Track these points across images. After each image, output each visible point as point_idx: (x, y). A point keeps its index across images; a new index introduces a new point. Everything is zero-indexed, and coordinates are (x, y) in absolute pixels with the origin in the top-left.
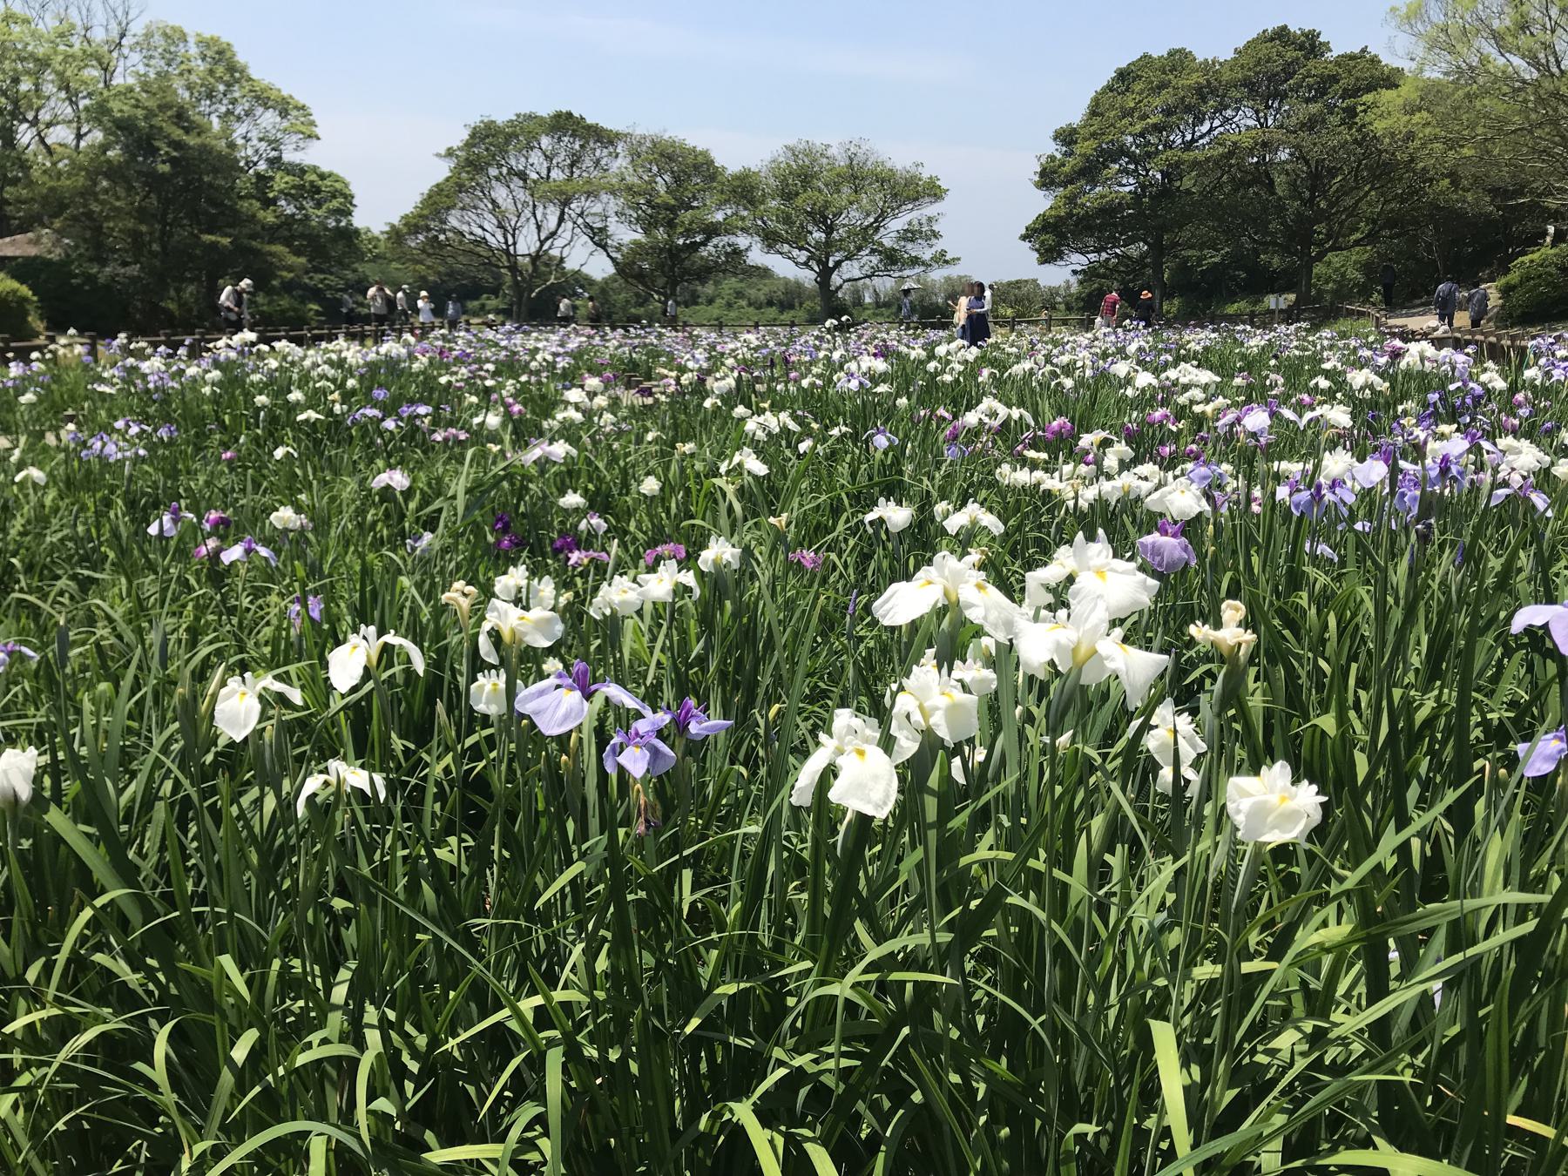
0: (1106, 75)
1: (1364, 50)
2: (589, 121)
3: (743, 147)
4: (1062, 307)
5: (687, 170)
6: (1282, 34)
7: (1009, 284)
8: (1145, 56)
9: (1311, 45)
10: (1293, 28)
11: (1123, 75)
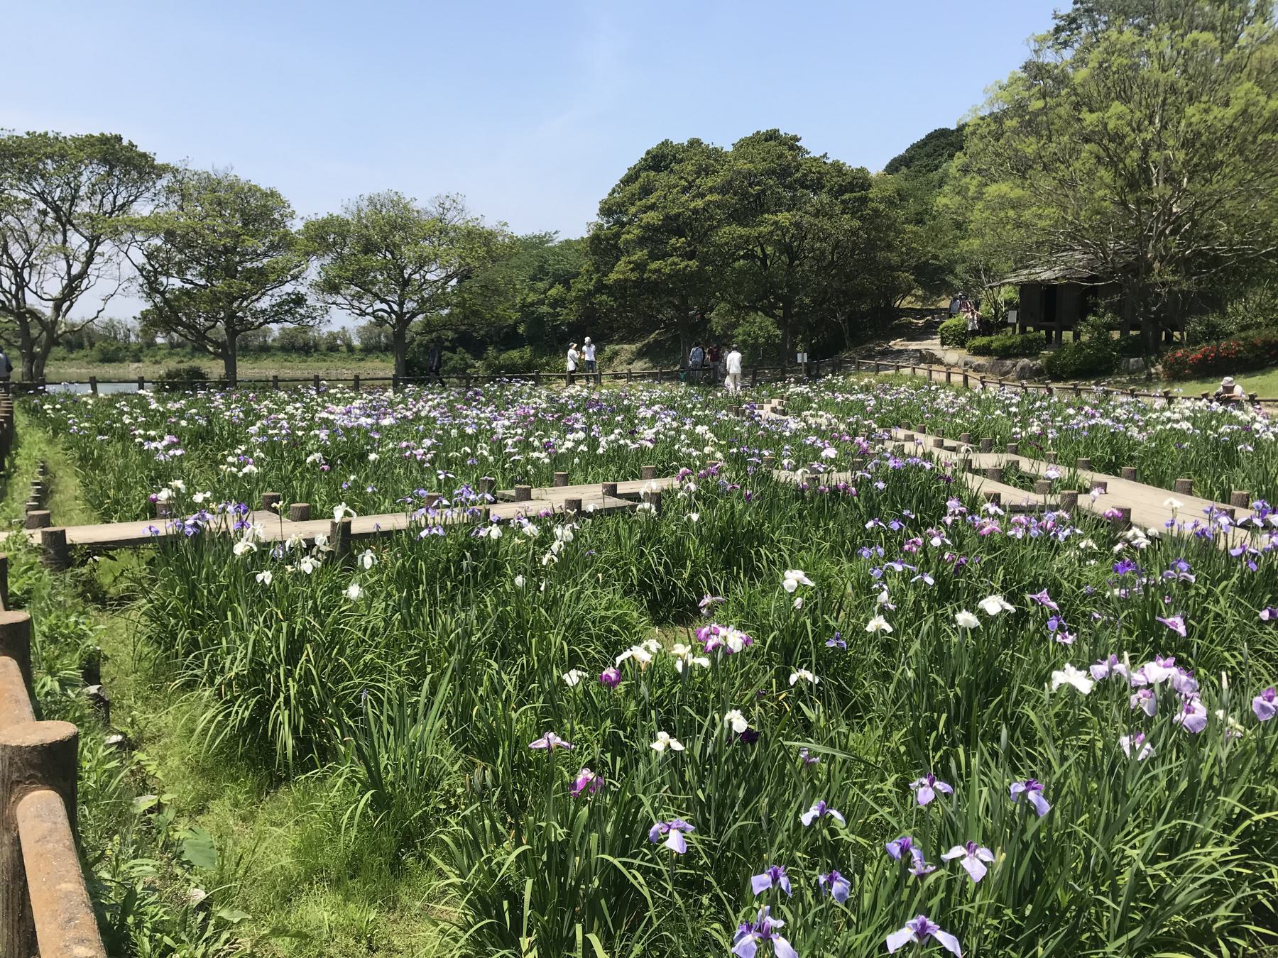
0: (635, 156)
1: (825, 156)
2: (141, 149)
3: (316, 192)
4: (344, 349)
5: (256, 211)
6: (772, 136)
8: (665, 144)
9: (792, 143)
10: (782, 133)
11: (660, 160)
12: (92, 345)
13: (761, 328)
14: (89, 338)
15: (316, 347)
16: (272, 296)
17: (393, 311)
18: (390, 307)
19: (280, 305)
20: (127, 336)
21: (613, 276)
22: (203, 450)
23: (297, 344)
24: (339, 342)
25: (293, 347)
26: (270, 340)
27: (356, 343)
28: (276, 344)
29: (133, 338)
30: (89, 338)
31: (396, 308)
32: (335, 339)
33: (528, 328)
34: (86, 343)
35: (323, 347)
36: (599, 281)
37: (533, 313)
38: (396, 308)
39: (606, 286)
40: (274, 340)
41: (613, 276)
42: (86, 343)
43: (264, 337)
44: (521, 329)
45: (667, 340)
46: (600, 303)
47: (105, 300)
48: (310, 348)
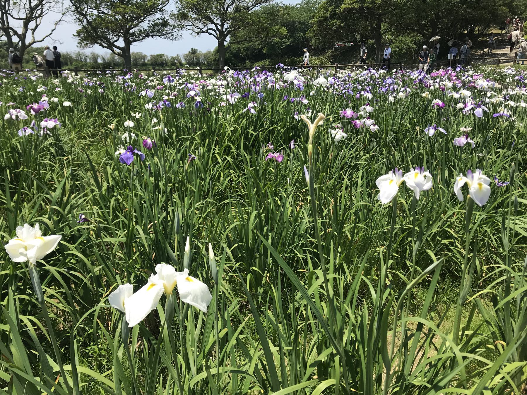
4: (178, 64)
7: (157, 56)
12: (71, 64)
13: (405, 44)
14: (70, 60)
15: (166, 64)
16: (149, 21)
17: (218, 29)
18: (217, 27)
19: (154, 26)
20: (86, 60)
21: (343, 7)
22: (99, 115)
23: (158, 63)
24: (176, 61)
25: (156, 64)
26: (146, 61)
27: (183, 62)
28: (149, 63)
29: (88, 60)
30: (70, 60)
31: (219, 27)
32: (174, 60)
33: (268, 50)
34: (69, 63)
35: (169, 64)
36: (333, 11)
37: (271, 42)
38: (219, 27)
39: (336, 14)
40: (148, 61)
41: (343, 7)
42: (69, 63)
43: (144, 59)
44: (264, 51)
45: (338, 54)
46: (333, 25)
47: (56, 24)
48: (164, 64)
